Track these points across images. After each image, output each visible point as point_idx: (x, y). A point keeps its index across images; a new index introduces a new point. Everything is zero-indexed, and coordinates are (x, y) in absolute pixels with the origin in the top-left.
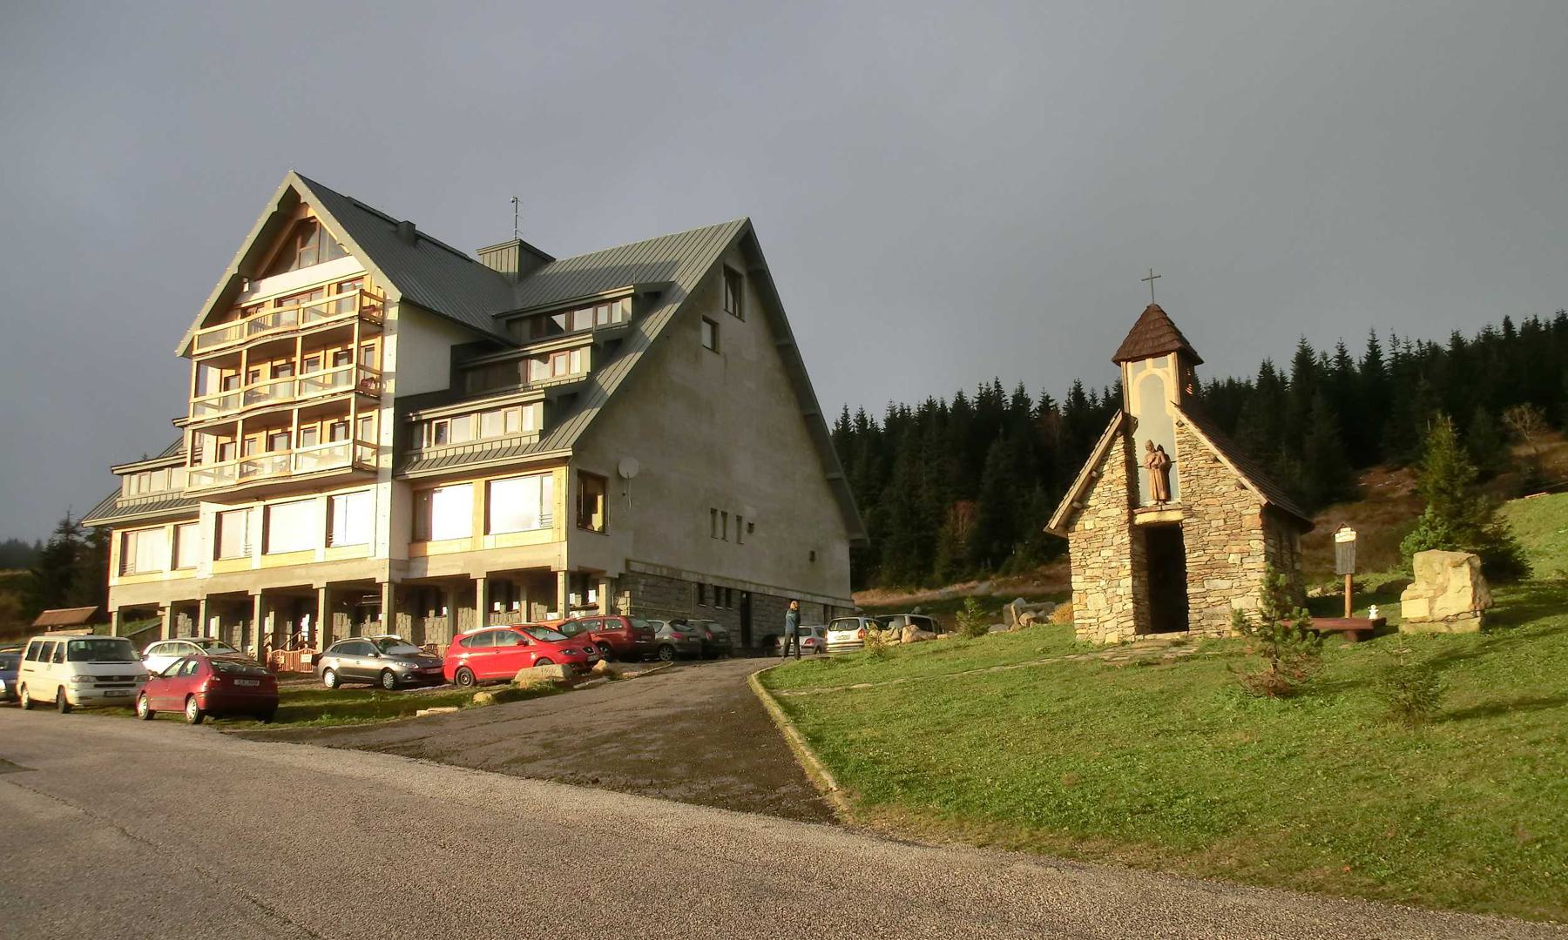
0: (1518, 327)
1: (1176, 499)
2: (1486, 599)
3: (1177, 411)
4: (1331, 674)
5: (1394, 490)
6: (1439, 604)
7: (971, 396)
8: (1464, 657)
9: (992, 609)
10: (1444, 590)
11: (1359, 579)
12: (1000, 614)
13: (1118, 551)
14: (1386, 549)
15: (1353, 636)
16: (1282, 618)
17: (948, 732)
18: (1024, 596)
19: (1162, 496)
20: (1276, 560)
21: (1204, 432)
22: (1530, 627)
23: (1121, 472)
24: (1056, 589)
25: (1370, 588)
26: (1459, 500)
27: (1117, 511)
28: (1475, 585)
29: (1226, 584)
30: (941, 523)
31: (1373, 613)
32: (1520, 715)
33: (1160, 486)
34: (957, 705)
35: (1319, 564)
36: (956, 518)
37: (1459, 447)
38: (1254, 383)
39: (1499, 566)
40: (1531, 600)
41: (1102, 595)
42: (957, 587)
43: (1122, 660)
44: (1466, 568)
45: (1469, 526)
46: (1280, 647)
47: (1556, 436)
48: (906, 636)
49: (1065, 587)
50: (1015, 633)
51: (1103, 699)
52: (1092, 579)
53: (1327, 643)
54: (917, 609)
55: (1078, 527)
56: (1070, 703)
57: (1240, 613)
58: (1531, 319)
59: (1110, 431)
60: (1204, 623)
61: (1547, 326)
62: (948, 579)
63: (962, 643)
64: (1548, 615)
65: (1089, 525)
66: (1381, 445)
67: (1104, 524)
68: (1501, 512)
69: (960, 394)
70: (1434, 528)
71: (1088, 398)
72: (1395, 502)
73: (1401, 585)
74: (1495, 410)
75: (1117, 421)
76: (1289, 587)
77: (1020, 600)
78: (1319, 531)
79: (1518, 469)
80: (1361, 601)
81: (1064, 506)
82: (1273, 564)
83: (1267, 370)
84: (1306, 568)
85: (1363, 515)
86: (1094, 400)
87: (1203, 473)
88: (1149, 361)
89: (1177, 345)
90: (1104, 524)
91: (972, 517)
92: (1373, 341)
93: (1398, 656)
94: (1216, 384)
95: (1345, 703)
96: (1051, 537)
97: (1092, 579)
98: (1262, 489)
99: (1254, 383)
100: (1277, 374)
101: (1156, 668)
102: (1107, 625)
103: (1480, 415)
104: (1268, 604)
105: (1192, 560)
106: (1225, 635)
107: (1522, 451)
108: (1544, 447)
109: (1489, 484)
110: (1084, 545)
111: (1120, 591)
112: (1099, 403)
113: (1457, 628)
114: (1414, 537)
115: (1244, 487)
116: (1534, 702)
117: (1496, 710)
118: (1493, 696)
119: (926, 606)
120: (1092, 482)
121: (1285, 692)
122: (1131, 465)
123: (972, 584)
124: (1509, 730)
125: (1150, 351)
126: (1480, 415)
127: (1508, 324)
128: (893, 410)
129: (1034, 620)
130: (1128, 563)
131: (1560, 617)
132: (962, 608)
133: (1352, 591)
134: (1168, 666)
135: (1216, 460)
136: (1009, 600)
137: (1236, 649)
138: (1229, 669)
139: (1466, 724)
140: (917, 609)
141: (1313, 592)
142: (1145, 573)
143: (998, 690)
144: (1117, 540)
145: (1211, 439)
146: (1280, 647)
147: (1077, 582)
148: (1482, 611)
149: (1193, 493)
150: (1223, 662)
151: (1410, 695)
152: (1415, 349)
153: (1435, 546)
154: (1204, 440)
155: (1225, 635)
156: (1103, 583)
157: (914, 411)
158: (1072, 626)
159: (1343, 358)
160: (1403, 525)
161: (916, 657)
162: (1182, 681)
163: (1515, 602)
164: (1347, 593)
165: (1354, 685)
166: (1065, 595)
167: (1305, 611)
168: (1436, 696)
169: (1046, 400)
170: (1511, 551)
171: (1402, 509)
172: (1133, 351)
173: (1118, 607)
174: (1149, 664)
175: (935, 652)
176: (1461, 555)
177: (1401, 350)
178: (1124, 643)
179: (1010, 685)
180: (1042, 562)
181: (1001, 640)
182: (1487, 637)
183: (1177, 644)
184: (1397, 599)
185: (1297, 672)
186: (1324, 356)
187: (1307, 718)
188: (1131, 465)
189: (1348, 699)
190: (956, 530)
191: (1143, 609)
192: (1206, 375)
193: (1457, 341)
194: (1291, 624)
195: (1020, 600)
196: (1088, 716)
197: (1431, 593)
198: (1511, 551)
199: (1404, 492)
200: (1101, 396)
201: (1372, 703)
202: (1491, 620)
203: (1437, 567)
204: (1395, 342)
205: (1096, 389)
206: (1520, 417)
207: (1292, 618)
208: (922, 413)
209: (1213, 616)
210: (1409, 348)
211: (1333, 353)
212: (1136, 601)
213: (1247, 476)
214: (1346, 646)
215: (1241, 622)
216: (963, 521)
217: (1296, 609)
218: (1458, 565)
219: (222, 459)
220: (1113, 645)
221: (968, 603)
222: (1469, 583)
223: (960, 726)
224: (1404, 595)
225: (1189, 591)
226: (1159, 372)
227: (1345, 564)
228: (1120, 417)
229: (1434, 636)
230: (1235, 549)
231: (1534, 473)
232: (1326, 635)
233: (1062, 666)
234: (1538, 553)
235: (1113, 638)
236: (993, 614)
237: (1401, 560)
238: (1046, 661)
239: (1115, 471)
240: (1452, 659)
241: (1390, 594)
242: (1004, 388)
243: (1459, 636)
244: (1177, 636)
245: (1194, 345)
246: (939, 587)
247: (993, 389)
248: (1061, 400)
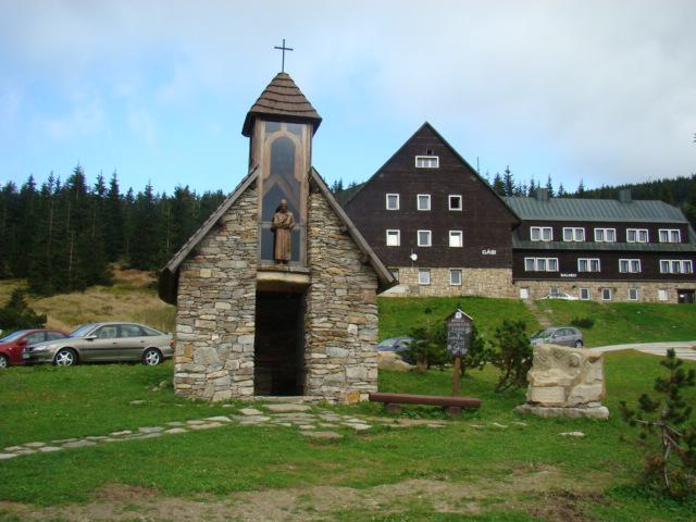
6: (574, 392)
29: (342, 352)
58: (338, 181)
90: (223, 275)
193: (164, 195)
230: (355, 320)
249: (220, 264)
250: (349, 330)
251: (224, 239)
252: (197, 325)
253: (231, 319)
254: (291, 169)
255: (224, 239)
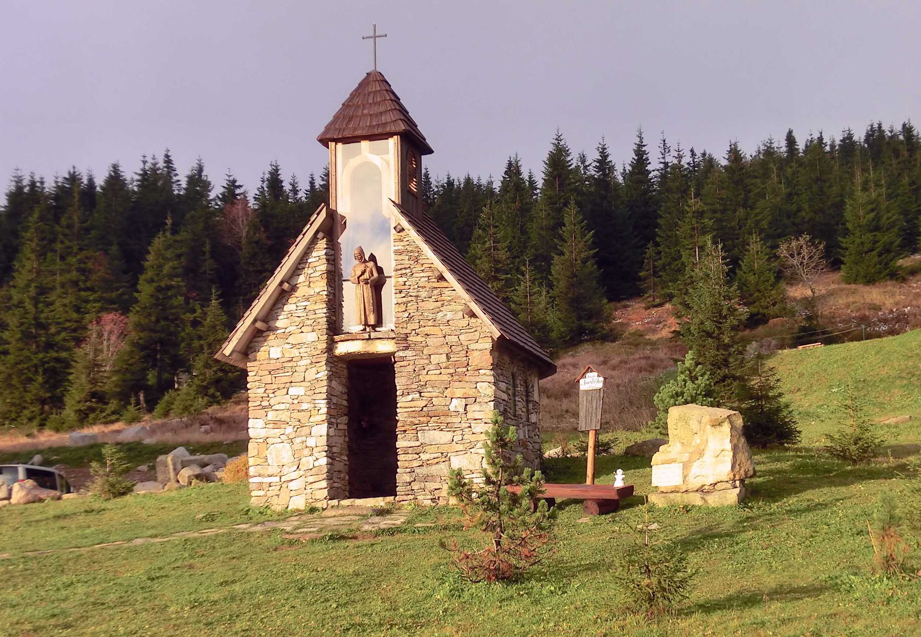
0: (801, 145)
1: (389, 323)
2: (747, 466)
3: (396, 211)
4: (564, 553)
5: (654, 331)
6: (695, 469)
7: (131, 173)
8: (719, 536)
9: (140, 459)
10: (701, 454)
11: (604, 438)
12: (153, 468)
13: (312, 389)
14: (637, 403)
15: (594, 507)
16: (510, 482)
17: (67, 626)
18: (186, 445)
19: (372, 320)
20: (506, 411)
21: (428, 241)
22: (792, 501)
23: (321, 286)
24: (230, 437)
25: (618, 450)
26: (727, 347)
27: (311, 337)
28: (735, 449)
29: (446, 437)
30: (79, 341)
31: (619, 480)
32: (776, 606)
33: (370, 307)
34: (81, 589)
35: (560, 417)
36: (100, 335)
37: (729, 283)
38: (497, 186)
39: (764, 429)
40: (798, 469)
41: (287, 442)
42: (95, 430)
43: (312, 529)
44: (726, 427)
45: (735, 378)
46: (505, 519)
47: (837, 276)
48: (18, 494)
49: (241, 436)
50: (168, 496)
51: (281, 583)
52: (277, 424)
53: (563, 516)
54: (37, 458)
55: (261, 355)
56: (237, 588)
57: (459, 474)
58: (816, 136)
59: (310, 231)
60: (415, 486)
61: (832, 146)
62: (84, 418)
63: (96, 506)
64: (813, 487)
65: (275, 353)
66: (642, 274)
67: (295, 353)
68: (770, 363)
69: (115, 167)
70: (693, 379)
71: (287, 187)
72: (653, 344)
73: (655, 446)
74: (774, 235)
75: (319, 219)
76: (522, 444)
77: (181, 450)
78: (560, 377)
79: (792, 313)
80: (605, 466)
81: (244, 326)
82: (504, 413)
83: (513, 170)
84: (546, 422)
85: (615, 360)
86: (295, 191)
87: (423, 294)
88: (365, 144)
89: (402, 127)
90: (295, 353)
91: (123, 335)
92: (640, 146)
93: (641, 532)
94: (450, 183)
95: (581, 591)
96: (225, 367)
97: (277, 424)
98: (495, 319)
99: (497, 186)
100: (525, 176)
101: (350, 544)
102: (292, 485)
103: (755, 245)
104: (493, 463)
105: (406, 405)
106: (442, 503)
107: (797, 292)
108: (821, 290)
109: (761, 330)
110: (268, 379)
111: (311, 442)
112: (302, 195)
113: (713, 500)
114: (670, 387)
115: (473, 315)
116: (793, 591)
117: (750, 600)
118: (748, 583)
119: (52, 454)
120: (283, 296)
121: (508, 576)
122: (334, 278)
123: (116, 426)
124: (763, 623)
125: (365, 133)
126: (755, 245)
127: (791, 140)
128: (19, 180)
129: (197, 477)
130: (323, 406)
131: (826, 490)
132: (100, 458)
133: (597, 452)
134: (366, 542)
135: (441, 278)
136: (166, 449)
137: (452, 521)
138: (443, 545)
139: (715, 617)
140: (37, 458)
141: (552, 452)
142: (345, 419)
143: (138, 571)
144: (311, 374)
145: (437, 251)
146: (505, 519)
147: (256, 428)
148: (742, 481)
149: (410, 318)
150: (436, 536)
151: (654, 580)
152: (686, 160)
153: (693, 400)
154: (428, 252)
155: (442, 503)
156: (289, 430)
157: (49, 186)
158: (247, 486)
159: (604, 163)
160: (660, 373)
161: (29, 524)
162: (384, 560)
163: (779, 472)
164: (590, 454)
165: (592, 568)
166: (239, 447)
167: (538, 473)
168: (683, 581)
169: (232, 186)
170: (779, 410)
171: (662, 354)
172: (343, 131)
173: (308, 462)
174: (343, 538)
175: (57, 517)
176: (723, 412)
177: (671, 159)
178: (313, 510)
179: (158, 563)
180: (213, 401)
181: (150, 503)
182: (747, 513)
183: (381, 512)
184: (646, 462)
185: (525, 551)
186: (583, 159)
187: (533, 609)
188: (334, 278)
189: (583, 585)
190: (97, 351)
191: (339, 466)
192: (439, 169)
193: (735, 154)
194: (520, 490)
195: (181, 450)
196: (258, 606)
197: (686, 457)
198: (779, 410)
199: (665, 333)
200: (304, 187)
201: (612, 590)
202: (752, 492)
203: (694, 425)
204: (665, 149)
205: (298, 176)
206: (797, 250)
207: (522, 482)
208: (60, 189)
209: (426, 478)
210: (680, 157)
211: (593, 156)
212: (331, 455)
213: (477, 301)
214: (586, 520)
215: (460, 485)
216: (108, 342)
217: (527, 471)
218: (717, 424)
219: (691, 308)
220: (299, 513)
221: (106, 451)
222: (729, 446)
223: (84, 618)
224: (656, 458)
225: (399, 444)
226: (376, 160)
227: (589, 418)
228: (323, 214)
229: (687, 509)
230: (459, 393)
231: (809, 318)
232: (562, 506)
233: (231, 539)
234: (808, 414)
235: (298, 503)
236: (144, 468)
237: (656, 416)
238: (210, 533)
239: (312, 285)
240: (706, 538)
241: (639, 457)
242: (176, 165)
243: (716, 510)
244: (380, 502)
245: (423, 128)
246: (71, 428)
247: (161, 164)
248: (252, 187)
249: (291, 340)
250: (452, 408)
251: (293, 307)
252: (269, 418)
253: (304, 406)
254: (519, 173)
255: (293, 307)
